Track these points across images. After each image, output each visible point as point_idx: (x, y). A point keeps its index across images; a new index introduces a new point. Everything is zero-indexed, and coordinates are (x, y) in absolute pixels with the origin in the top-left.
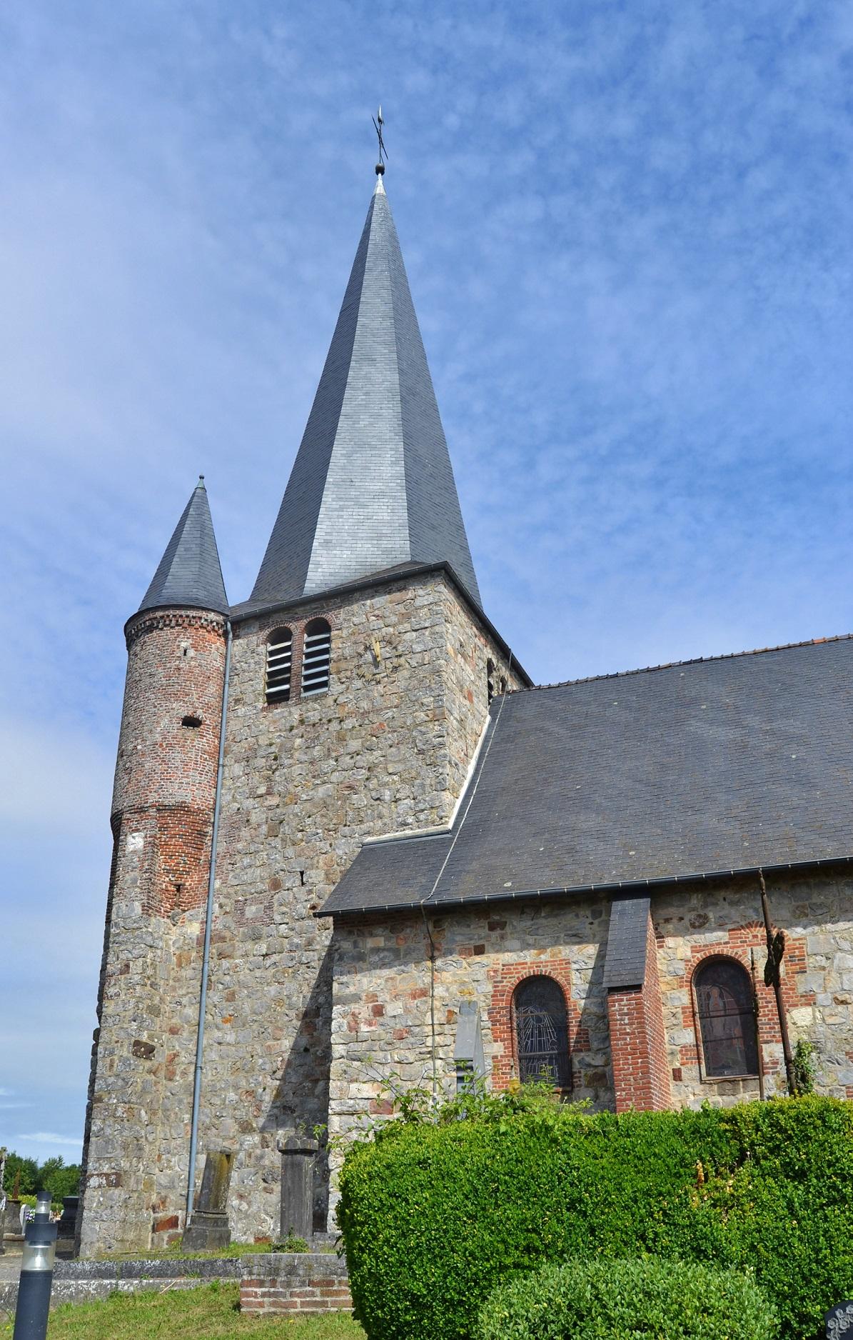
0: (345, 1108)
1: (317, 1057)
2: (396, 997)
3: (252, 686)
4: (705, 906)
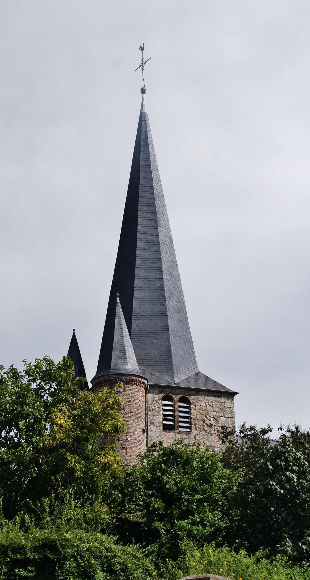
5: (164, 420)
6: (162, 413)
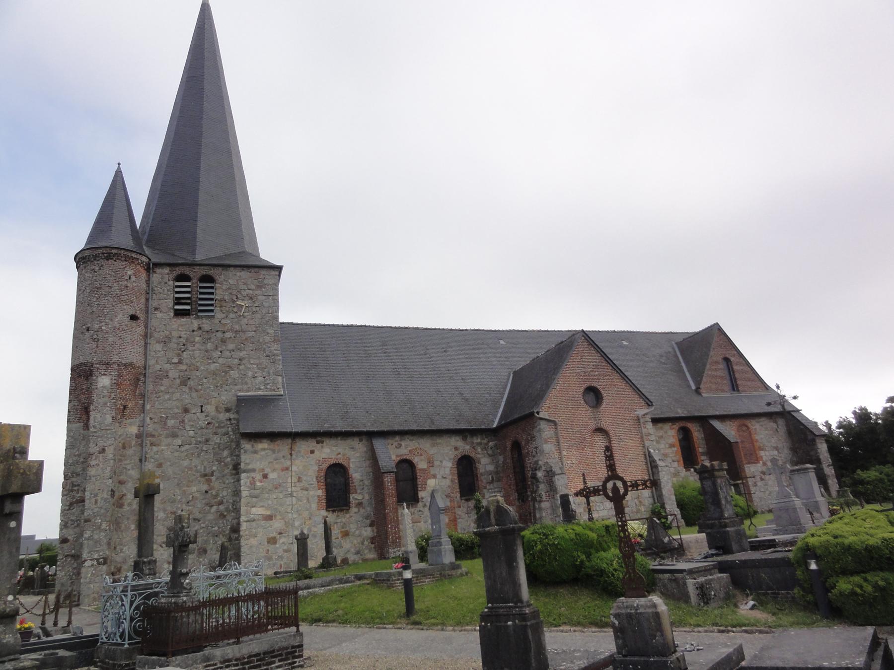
0: (249, 519)
1: (212, 495)
2: (274, 470)
3: (166, 302)
4: (401, 440)
5: (176, 304)
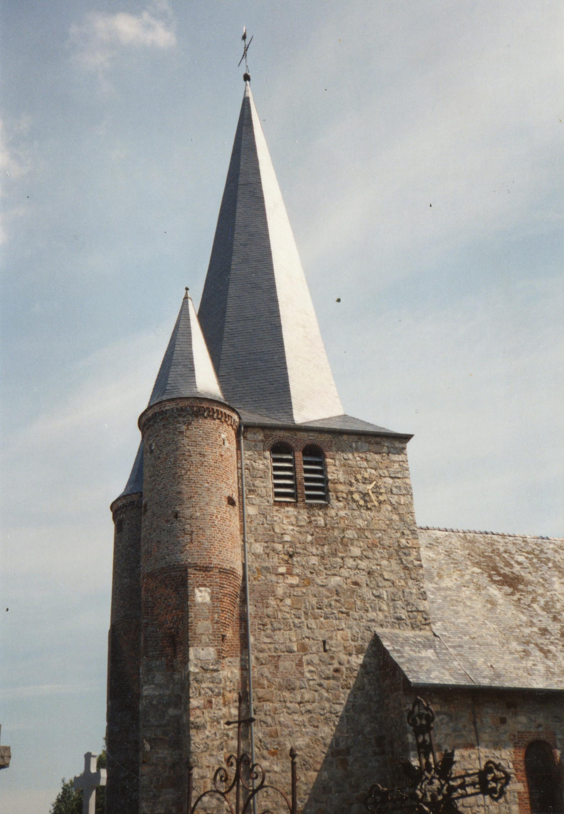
6: (272, 474)
